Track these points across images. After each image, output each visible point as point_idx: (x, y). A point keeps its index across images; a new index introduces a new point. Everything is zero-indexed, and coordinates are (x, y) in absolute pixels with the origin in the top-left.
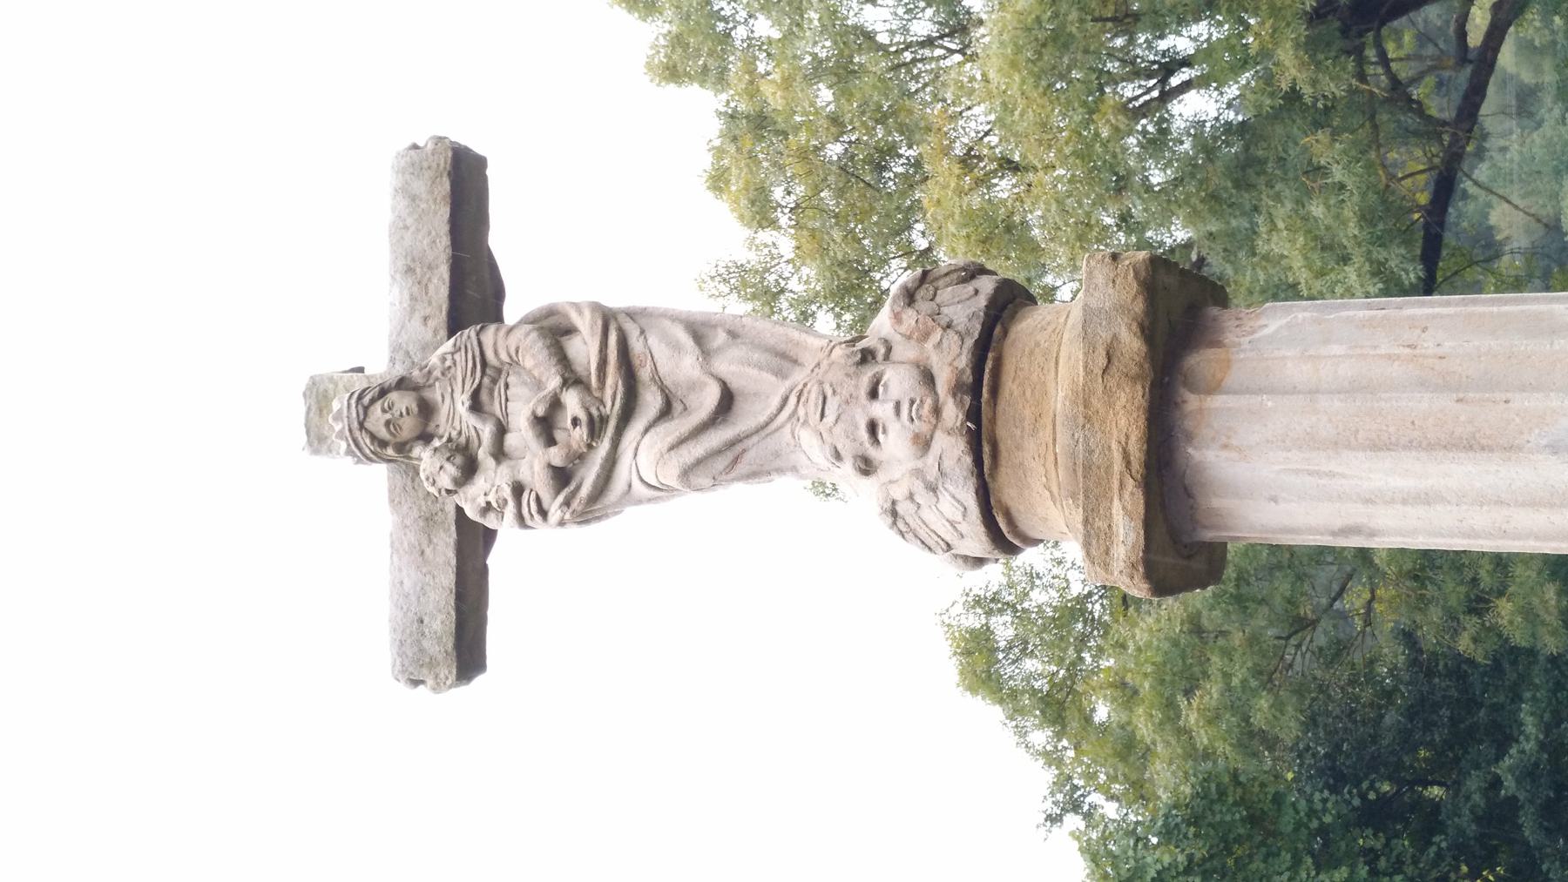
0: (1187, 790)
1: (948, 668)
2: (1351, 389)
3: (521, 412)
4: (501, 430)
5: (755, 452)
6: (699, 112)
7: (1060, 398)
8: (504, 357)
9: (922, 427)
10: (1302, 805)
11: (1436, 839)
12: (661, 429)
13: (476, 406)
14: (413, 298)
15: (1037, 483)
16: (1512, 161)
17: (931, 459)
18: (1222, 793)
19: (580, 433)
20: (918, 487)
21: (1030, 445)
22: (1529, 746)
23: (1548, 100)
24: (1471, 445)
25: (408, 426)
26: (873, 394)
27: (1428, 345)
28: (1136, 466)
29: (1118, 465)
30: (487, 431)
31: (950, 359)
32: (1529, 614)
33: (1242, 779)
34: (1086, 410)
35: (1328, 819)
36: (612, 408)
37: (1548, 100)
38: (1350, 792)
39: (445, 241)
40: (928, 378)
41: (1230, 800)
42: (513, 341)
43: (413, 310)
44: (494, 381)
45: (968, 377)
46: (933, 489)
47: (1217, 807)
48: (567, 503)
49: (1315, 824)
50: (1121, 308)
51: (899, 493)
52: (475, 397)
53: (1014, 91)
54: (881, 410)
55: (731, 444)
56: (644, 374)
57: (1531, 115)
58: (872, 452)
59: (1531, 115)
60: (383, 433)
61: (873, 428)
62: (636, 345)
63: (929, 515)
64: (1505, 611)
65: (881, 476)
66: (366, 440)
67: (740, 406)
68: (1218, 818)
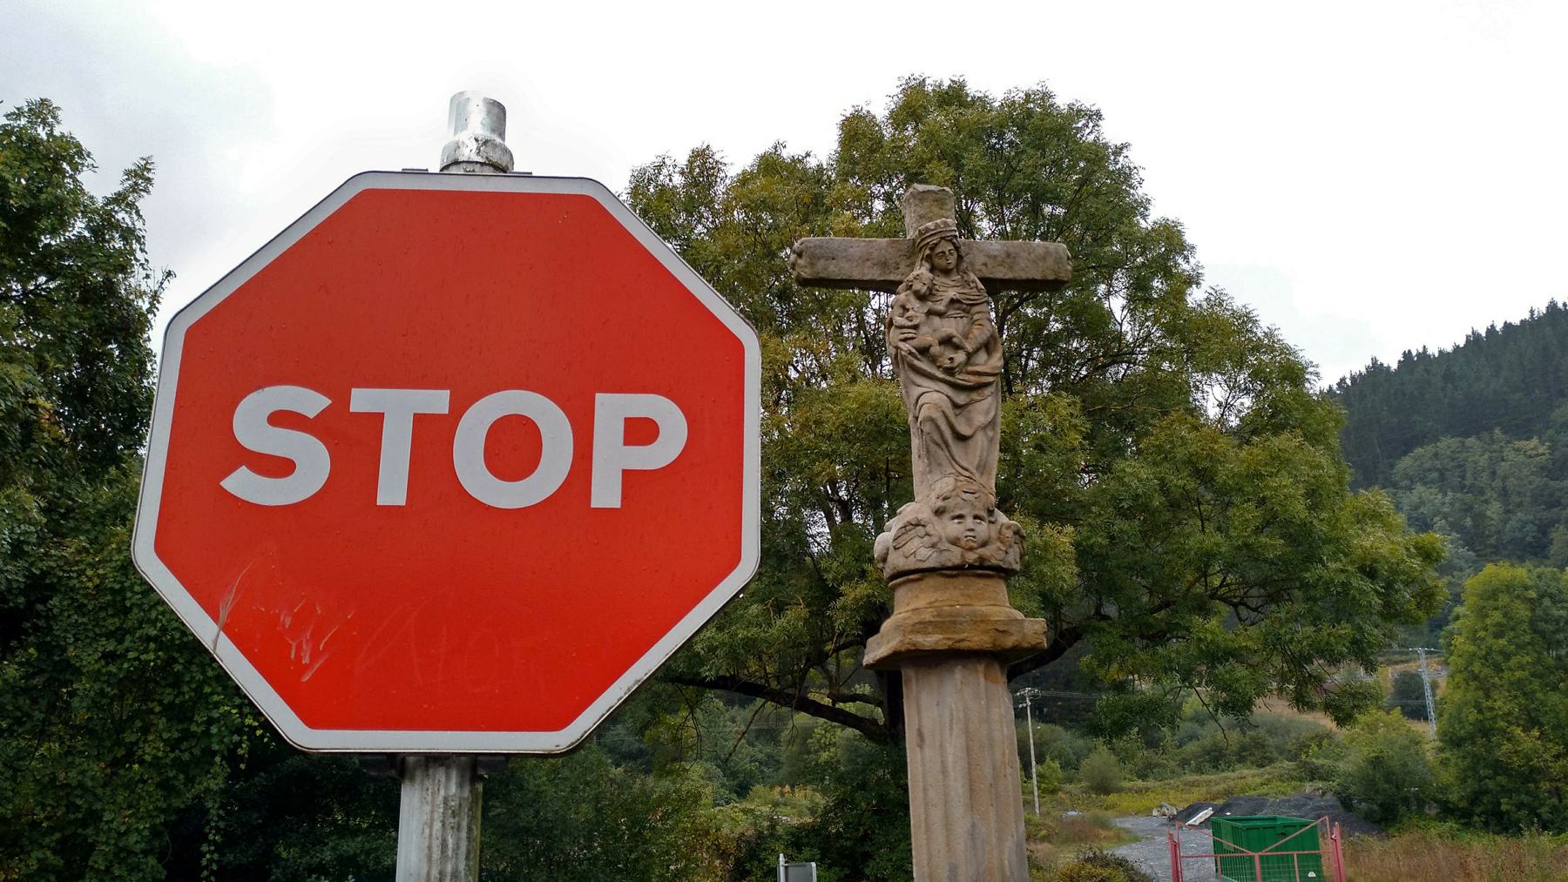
3: (950, 327)
4: (941, 315)
5: (942, 454)
6: (819, 145)
7: (982, 608)
9: (963, 543)
13: (953, 301)
15: (933, 596)
17: (948, 545)
19: (947, 364)
20: (935, 539)
21: (957, 593)
23: (768, 750)
25: (941, 262)
26: (976, 517)
27: (1009, 770)
29: (957, 637)
30: (940, 307)
31: (993, 553)
34: (980, 621)
36: (961, 379)
37: (768, 750)
39: (1024, 276)
40: (984, 544)
43: (989, 256)
46: (933, 546)
48: (911, 353)
51: (929, 529)
52: (958, 301)
53: (846, 404)
55: (946, 443)
56: (975, 396)
58: (947, 516)
60: (938, 250)
61: (961, 517)
62: (987, 391)
63: (917, 542)
66: (934, 240)
67: (961, 444)
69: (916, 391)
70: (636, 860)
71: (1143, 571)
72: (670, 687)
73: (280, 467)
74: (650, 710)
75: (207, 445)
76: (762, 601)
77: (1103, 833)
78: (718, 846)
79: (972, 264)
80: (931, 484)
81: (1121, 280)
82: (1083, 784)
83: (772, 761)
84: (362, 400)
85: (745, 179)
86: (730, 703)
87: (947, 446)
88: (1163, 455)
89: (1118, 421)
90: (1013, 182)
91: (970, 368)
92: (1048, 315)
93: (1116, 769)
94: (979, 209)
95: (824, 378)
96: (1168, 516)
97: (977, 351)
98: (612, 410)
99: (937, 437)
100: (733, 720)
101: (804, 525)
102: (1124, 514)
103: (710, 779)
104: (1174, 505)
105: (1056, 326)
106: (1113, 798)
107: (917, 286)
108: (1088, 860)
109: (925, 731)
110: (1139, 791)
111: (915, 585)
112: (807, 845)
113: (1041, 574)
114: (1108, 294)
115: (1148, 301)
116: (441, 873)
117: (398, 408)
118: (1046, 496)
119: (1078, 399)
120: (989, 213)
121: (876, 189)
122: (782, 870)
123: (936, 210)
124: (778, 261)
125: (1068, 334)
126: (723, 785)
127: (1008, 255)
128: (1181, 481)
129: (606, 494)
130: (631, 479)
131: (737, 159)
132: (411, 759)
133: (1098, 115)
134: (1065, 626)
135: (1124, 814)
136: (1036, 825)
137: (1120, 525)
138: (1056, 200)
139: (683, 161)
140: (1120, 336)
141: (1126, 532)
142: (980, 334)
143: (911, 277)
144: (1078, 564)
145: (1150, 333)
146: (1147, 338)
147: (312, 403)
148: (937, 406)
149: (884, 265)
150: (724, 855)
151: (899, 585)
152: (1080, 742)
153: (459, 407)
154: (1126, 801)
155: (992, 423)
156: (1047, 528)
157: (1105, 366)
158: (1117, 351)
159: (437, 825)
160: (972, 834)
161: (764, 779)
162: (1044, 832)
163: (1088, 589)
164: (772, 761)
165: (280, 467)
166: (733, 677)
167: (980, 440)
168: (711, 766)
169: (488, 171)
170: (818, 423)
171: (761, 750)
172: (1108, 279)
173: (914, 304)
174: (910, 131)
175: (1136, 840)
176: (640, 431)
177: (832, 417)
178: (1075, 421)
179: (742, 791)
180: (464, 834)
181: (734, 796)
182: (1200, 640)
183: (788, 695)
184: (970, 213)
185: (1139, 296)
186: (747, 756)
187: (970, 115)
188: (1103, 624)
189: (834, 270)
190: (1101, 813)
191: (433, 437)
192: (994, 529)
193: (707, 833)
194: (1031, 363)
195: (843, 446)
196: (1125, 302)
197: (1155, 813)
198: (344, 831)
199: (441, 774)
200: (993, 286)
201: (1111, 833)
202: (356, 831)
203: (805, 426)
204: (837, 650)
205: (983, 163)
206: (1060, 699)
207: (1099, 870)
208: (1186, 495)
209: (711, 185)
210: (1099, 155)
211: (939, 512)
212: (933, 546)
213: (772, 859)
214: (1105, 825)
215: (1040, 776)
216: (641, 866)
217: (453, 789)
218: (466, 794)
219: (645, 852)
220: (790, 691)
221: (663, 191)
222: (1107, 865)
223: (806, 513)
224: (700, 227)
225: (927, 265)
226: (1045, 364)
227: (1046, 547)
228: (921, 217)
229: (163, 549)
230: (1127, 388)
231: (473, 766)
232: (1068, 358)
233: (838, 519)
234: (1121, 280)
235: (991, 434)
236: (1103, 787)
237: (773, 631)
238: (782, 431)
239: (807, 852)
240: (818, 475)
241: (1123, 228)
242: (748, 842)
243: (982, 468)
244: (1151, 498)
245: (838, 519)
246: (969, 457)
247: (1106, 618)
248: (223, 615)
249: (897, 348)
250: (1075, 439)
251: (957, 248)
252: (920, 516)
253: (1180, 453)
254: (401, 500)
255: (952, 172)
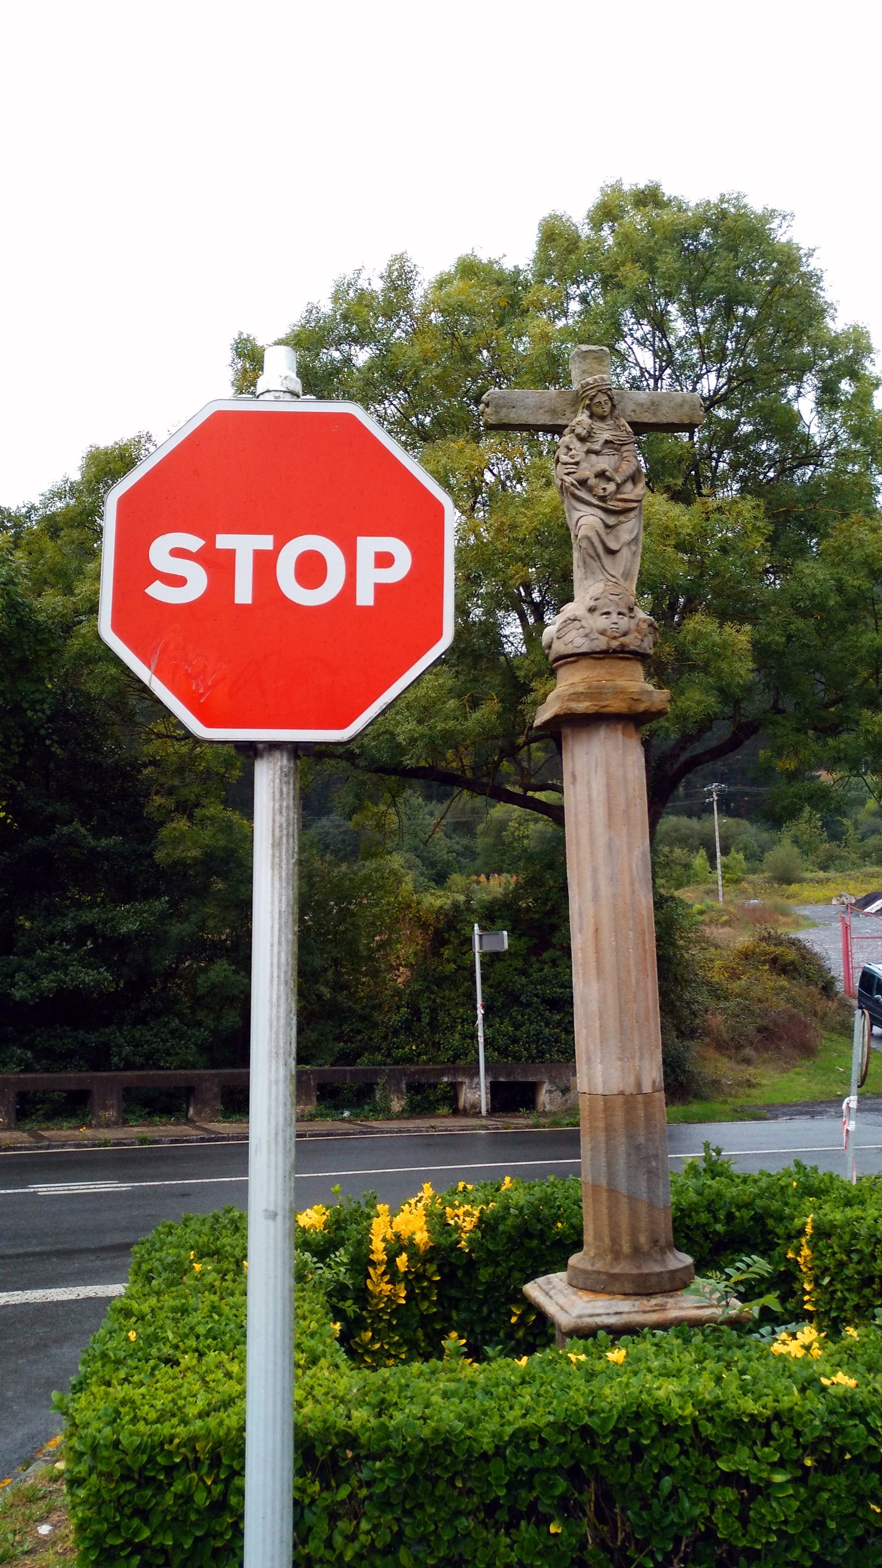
0: (41, 618)
1: (107, 439)
2: (625, 778)
3: (604, 463)
4: (597, 453)
5: (595, 565)
6: (518, 253)
7: (621, 682)
8: (625, 454)
9: (609, 633)
10: (38, 696)
11: (22, 784)
12: (602, 526)
13: (607, 442)
14: (642, 405)
16: (424, 819)
17: (597, 635)
18: (41, 642)
19: (601, 493)
20: (588, 631)
21: (603, 671)
22: (93, 843)
24: (610, 815)
25: (598, 410)
26: (619, 614)
27: (638, 801)
28: (602, 710)
30: (597, 447)
31: (632, 641)
32: (178, 841)
33: (54, 656)
34: (620, 692)
35: (30, 713)
36: (611, 505)
37: (465, 841)
38: (49, 728)
39: (665, 421)
40: (625, 634)
41: (38, 648)
42: (632, 459)
43: (638, 404)
44: (615, 449)
45: (627, 649)
46: (586, 636)
47: (32, 639)
48: (573, 484)
49: (25, 705)
50: (653, 703)
51: (584, 623)
52: (611, 442)
54: (614, 617)
55: (598, 556)
57: (454, 830)
58: (597, 613)
59: (454, 830)
60: (596, 400)
61: (608, 613)
62: (632, 514)
63: (574, 633)
64: (182, 824)
65: (588, 615)
66: (592, 393)
68: (25, 640)
69: (577, 515)
70: (344, 932)
71: (818, 668)
72: (375, 777)
73: (178, 581)
74: (357, 796)
75: (135, 571)
76: (459, 697)
77: (782, 919)
78: (419, 918)
79: (623, 411)
80: (587, 589)
81: (811, 381)
82: (766, 874)
83: (469, 853)
84: (223, 541)
85: (442, 283)
86: (428, 798)
87: (599, 558)
88: (840, 556)
89: (802, 524)
90: (705, 284)
91: (619, 496)
92: (739, 417)
93: (799, 861)
94: (673, 308)
95: (519, 481)
96: (842, 615)
97: (625, 482)
98: (368, 546)
99: (591, 551)
100: (431, 814)
101: (498, 626)
102: (804, 613)
103: (409, 868)
104: (850, 605)
105: (747, 429)
106: (795, 887)
107: (579, 430)
108: (763, 939)
109: (577, 773)
110: (820, 882)
111: (572, 665)
112: (500, 917)
113: (720, 671)
114: (799, 394)
115: (834, 404)
116: (281, 806)
117: (244, 546)
118: (729, 597)
119: (762, 502)
120: (683, 314)
121: (573, 290)
122: (477, 938)
123: (595, 366)
124: (474, 366)
125: (757, 436)
126: (422, 874)
127: (653, 403)
128: (856, 581)
129: (365, 597)
130: (381, 590)
131: (431, 266)
132: (261, 746)
133: (792, 215)
134: (743, 720)
135: (806, 902)
136: (719, 911)
137: (799, 623)
138: (749, 302)
139: (382, 268)
140: (806, 439)
141: (802, 631)
142: (627, 469)
143: (574, 423)
144: (755, 660)
145: (836, 436)
146: (834, 441)
147: (194, 543)
148: (592, 527)
149: (553, 412)
150: (424, 926)
151: (561, 665)
152: (765, 836)
153: (279, 545)
154: (807, 891)
155: (635, 540)
156: (728, 628)
157: (792, 469)
158: (808, 454)
159: (277, 781)
160: (610, 846)
161: (461, 870)
162: (725, 918)
163: (767, 685)
164: (469, 853)
165: (178, 581)
166: (432, 768)
167: (625, 553)
168: (411, 856)
169: (288, 397)
170: (513, 527)
171: (459, 842)
172: (798, 380)
173: (576, 444)
174: (606, 231)
175: (814, 925)
176: (384, 560)
177: (526, 522)
178: (759, 524)
179: (440, 879)
180: (291, 787)
181: (433, 884)
182: (867, 731)
183: (483, 784)
184: (665, 313)
185: (828, 398)
186: (443, 846)
187: (666, 216)
188: (779, 718)
189: (514, 417)
190: (780, 901)
191: (264, 563)
192: (633, 623)
193: (409, 906)
194: (721, 465)
195: (536, 549)
196: (813, 405)
197: (834, 902)
198: (79, 905)
199: (277, 754)
200: (638, 428)
201: (790, 920)
202: (92, 905)
203: (499, 531)
204: (528, 743)
205: (677, 265)
206: (747, 794)
207: (772, 948)
208: (861, 594)
209: (409, 289)
210: (789, 260)
211: (592, 610)
212: (586, 636)
213: (468, 929)
214: (785, 913)
215: (725, 867)
216: (349, 936)
217: (285, 762)
218: (292, 765)
219: (352, 924)
220: (485, 780)
221: (362, 295)
222: (781, 944)
223: (501, 614)
224: (398, 331)
225: (587, 413)
226: (734, 466)
227: (725, 645)
228: (584, 372)
229: (118, 627)
230: (812, 489)
231: (296, 750)
232: (757, 459)
233: (531, 620)
234: (811, 381)
235: (634, 548)
236: (786, 878)
237: (469, 724)
238: (478, 536)
239: (499, 922)
240: (511, 578)
241: (811, 332)
242: (446, 915)
243: (626, 575)
244: (827, 597)
245: (531, 620)
246: (616, 567)
247: (781, 712)
248: (153, 666)
249: (562, 480)
250: (758, 541)
251: (611, 399)
252: (577, 613)
253: (857, 555)
254: (249, 601)
255: (646, 275)
